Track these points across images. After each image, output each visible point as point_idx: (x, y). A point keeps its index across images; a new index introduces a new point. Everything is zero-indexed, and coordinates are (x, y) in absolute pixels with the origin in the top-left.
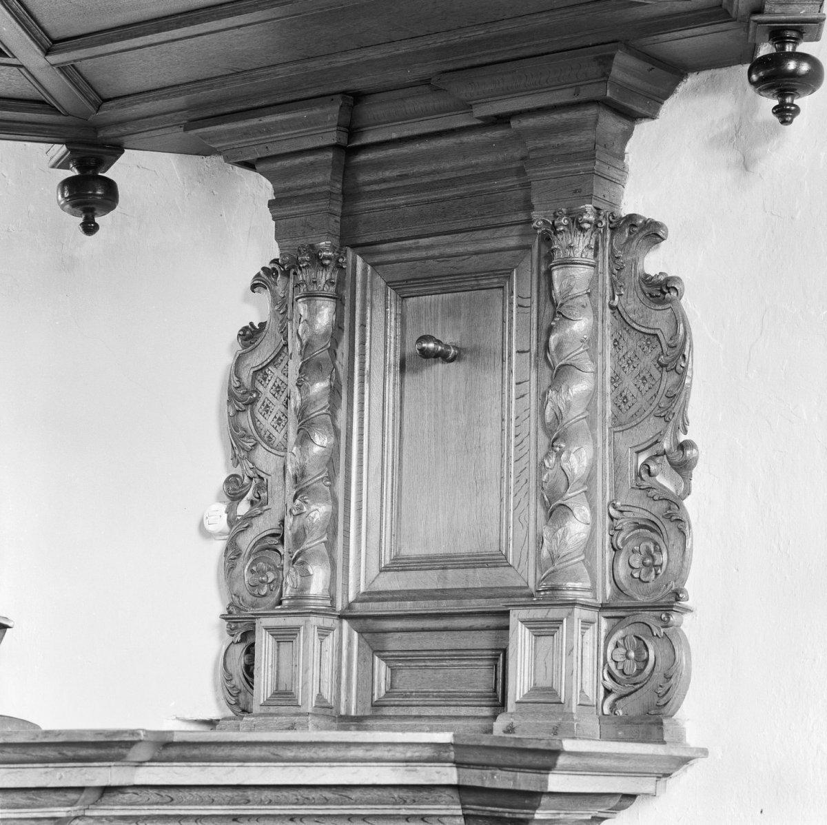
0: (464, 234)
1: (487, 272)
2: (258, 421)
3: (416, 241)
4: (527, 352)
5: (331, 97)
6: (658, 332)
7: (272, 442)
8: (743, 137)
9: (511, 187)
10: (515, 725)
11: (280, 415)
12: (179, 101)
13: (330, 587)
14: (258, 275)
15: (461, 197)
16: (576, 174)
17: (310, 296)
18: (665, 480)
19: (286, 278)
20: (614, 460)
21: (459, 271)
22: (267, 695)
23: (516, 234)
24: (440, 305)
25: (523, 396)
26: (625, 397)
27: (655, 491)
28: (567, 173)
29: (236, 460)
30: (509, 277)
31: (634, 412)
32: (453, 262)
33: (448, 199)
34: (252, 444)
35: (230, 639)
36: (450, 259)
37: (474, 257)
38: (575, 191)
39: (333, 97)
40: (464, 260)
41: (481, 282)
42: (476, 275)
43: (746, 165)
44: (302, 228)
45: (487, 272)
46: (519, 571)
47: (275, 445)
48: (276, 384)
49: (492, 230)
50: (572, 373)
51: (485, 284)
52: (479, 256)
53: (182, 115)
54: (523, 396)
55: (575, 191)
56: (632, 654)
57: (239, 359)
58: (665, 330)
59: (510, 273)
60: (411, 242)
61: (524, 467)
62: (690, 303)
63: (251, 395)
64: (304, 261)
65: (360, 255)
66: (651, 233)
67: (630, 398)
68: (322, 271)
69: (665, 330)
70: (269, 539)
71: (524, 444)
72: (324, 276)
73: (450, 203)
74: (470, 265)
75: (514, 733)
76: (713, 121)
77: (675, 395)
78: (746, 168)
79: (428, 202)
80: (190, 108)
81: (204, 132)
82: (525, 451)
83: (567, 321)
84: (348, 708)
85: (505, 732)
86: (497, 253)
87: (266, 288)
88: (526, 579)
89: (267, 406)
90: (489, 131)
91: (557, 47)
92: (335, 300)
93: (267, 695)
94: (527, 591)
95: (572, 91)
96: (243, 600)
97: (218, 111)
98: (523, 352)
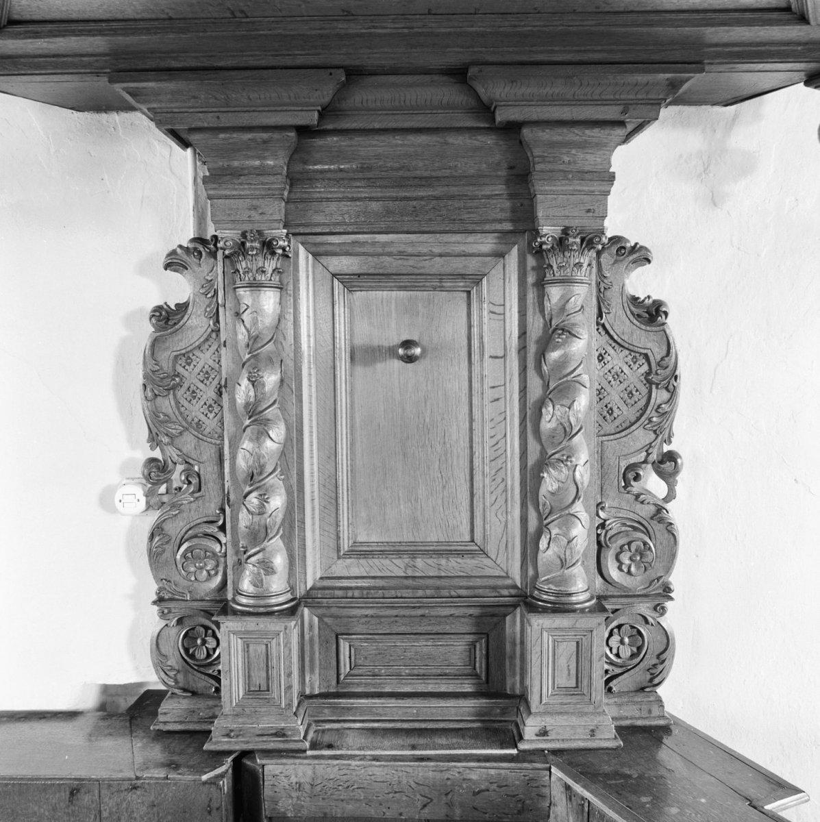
0: (430, 235)
1: (453, 275)
2: (183, 406)
3: (372, 236)
4: (501, 357)
5: (329, 71)
6: (650, 354)
7: (202, 429)
8: (711, 175)
9: (497, 195)
10: (548, 728)
11: (210, 402)
12: (96, 43)
13: (289, 578)
14: (173, 253)
15: (437, 198)
16: (591, 193)
17: (255, 286)
18: (654, 484)
19: (213, 260)
20: (602, 467)
21: (418, 272)
22: (239, 697)
23: (491, 242)
24: (393, 301)
25: (498, 400)
26: (611, 409)
27: (644, 496)
28: (580, 191)
29: (154, 440)
30: (478, 282)
31: (620, 422)
32: (411, 262)
33: (422, 198)
34: (178, 431)
35: (163, 623)
36: (409, 258)
37: (437, 259)
38: (589, 211)
39: (333, 71)
40: (426, 260)
41: (444, 284)
42: (441, 276)
43: (714, 200)
44: (247, 211)
45: (453, 275)
46: (498, 562)
47: (206, 432)
48: (183, 364)
49: (464, 235)
50: (579, 390)
51: (450, 287)
52: (443, 258)
53: (106, 61)
54: (498, 400)
55: (589, 211)
56: (626, 640)
57: (155, 344)
58: (656, 350)
59: (481, 280)
60: (366, 236)
61: (499, 467)
62: (674, 324)
63: (174, 380)
64: (252, 248)
65: (302, 244)
66: (638, 255)
67: (615, 409)
68: (270, 259)
69: (657, 352)
70: (204, 525)
71: (499, 445)
72: (270, 265)
73: (423, 203)
74: (432, 266)
75: (548, 736)
76: (681, 155)
77: (666, 412)
78: (715, 204)
79: (396, 199)
80: (115, 54)
81: (137, 88)
82: (500, 452)
83: (575, 339)
84: (312, 688)
85: (537, 735)
86: (464, 258)
87: (187, 269)
88: (505, 569)
89: (194, 392)
90: (480, 135)
91: (631, 57)
92: (279, 290)
93: (239, 697)
94: (508, 582)
95: (621, 108)
96: (176, 585)
97: (163, 64)
98: (496, 357)
